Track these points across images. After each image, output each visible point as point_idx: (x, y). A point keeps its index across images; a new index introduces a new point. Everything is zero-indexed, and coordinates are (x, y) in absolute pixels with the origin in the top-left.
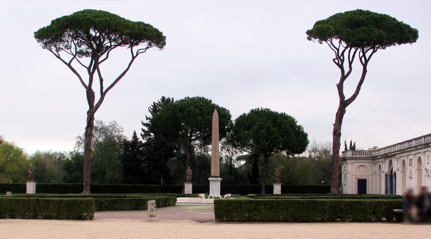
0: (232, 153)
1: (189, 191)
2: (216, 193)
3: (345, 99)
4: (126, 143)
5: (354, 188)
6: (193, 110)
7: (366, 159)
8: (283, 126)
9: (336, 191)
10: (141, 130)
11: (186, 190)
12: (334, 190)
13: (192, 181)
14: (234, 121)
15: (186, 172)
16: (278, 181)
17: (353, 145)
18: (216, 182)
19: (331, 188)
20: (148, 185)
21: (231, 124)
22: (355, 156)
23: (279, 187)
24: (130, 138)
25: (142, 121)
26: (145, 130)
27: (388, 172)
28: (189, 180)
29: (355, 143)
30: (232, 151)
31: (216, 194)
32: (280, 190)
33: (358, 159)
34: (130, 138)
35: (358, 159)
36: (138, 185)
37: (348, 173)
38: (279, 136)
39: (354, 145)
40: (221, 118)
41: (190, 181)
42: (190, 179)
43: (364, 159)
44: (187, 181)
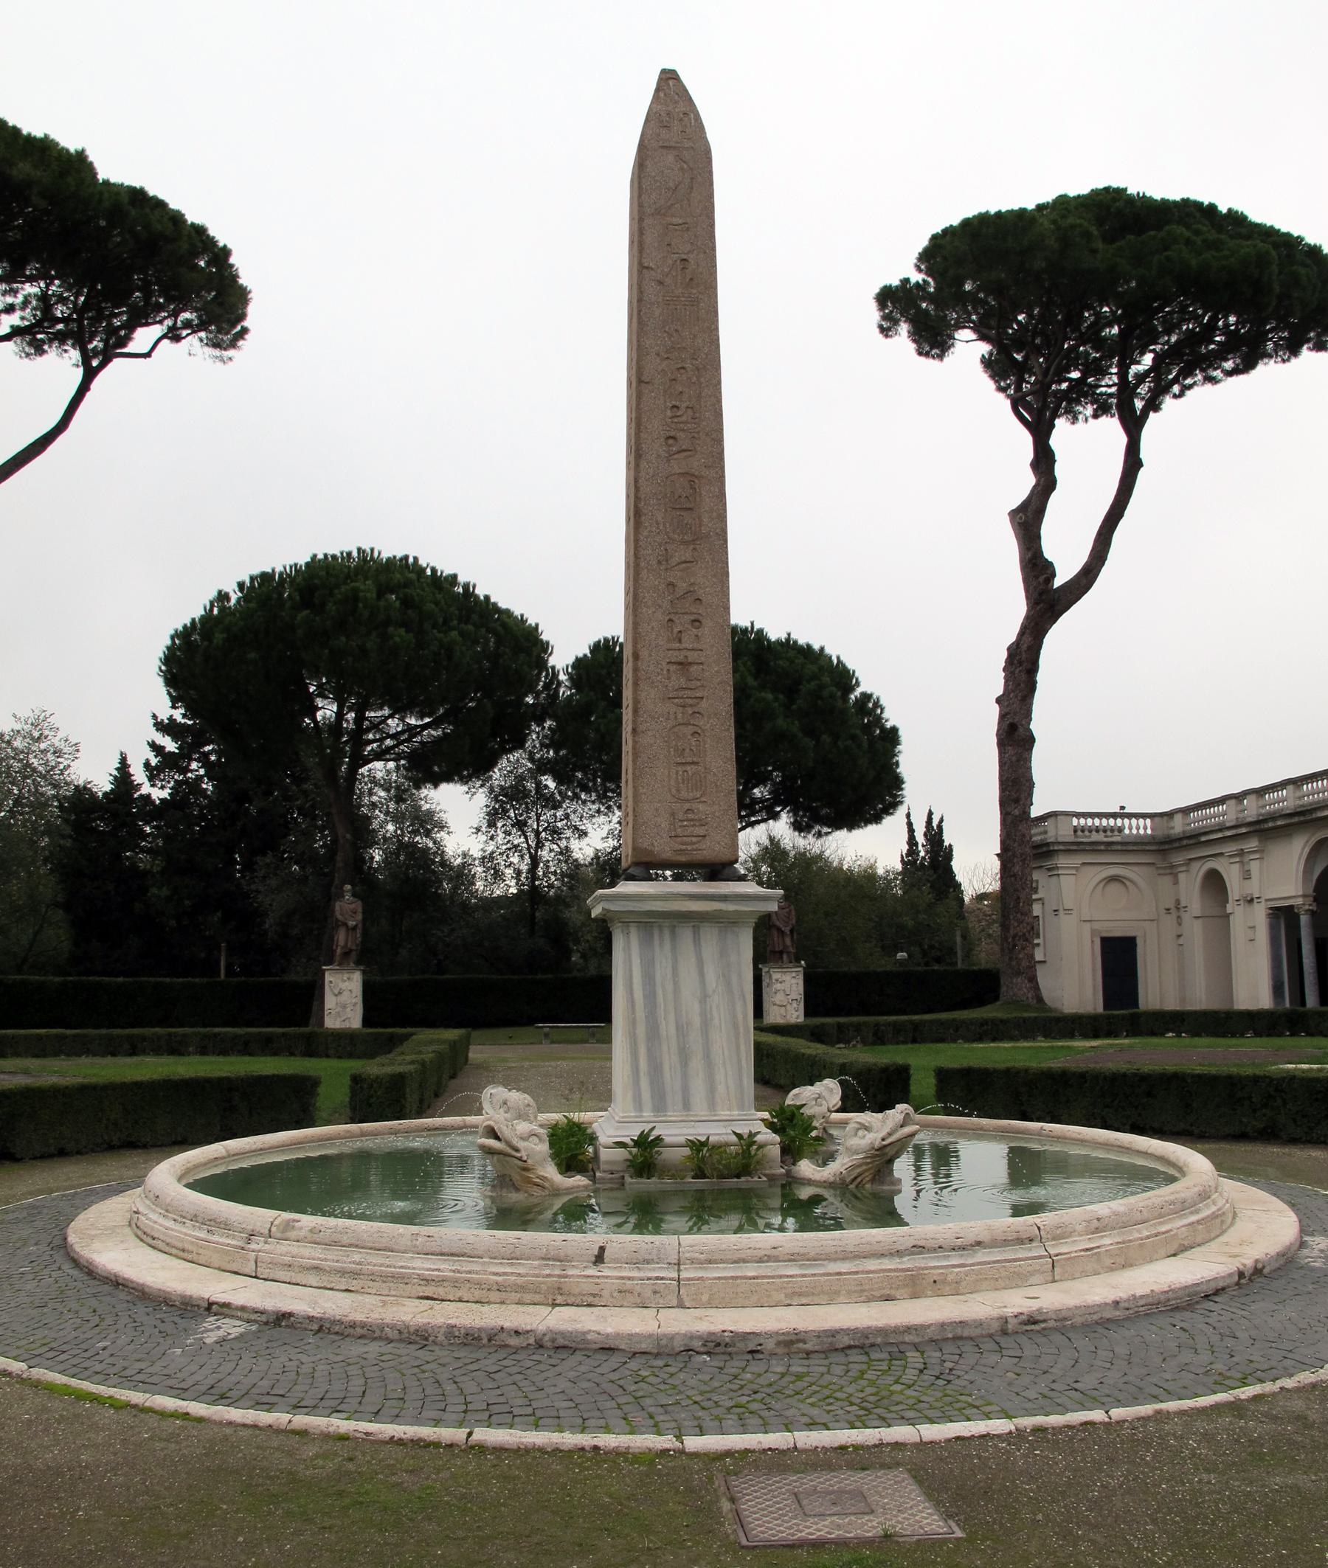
0: (537, 833)
1: (344, 1007)
2: (712, 1091)
3: (1058, 583)
4: (82, 799)
5: (1089, 983)
6: (368, 595)
7: (1135, 848)
8: (805, 688)
9: (1030, 995)
10: (148, 748)
11: (330, 1002)
12: (1013, 987)
13: (364, 957)
14: (561, 673)
15: (333, 911)
16: (788, 953)
17: (935, 824)
18: (686, 934)
19: (1004, 980)
20: (146, 979)
21: (551, 682)
22: (1086, 837)
23: (794, 981)
24: (103, 784)
25: (155, 716)
26: (163, 748)
27: (1304, 896)
28: (346, 954)
29: (941, 820)
30: (535, 827)
31: (712, 1105)
32: (798, 997)
33: (1102, 847)
34: (103, 784)
35: (1101, 850)
36: (97, 979)
37: (1061, 912)
38: (795, 727)
39: (940, 827)
40: (507, 650)
41: (354, 955)
42: (349, 944)
43: (1124, 848)
44: (337, 958)
